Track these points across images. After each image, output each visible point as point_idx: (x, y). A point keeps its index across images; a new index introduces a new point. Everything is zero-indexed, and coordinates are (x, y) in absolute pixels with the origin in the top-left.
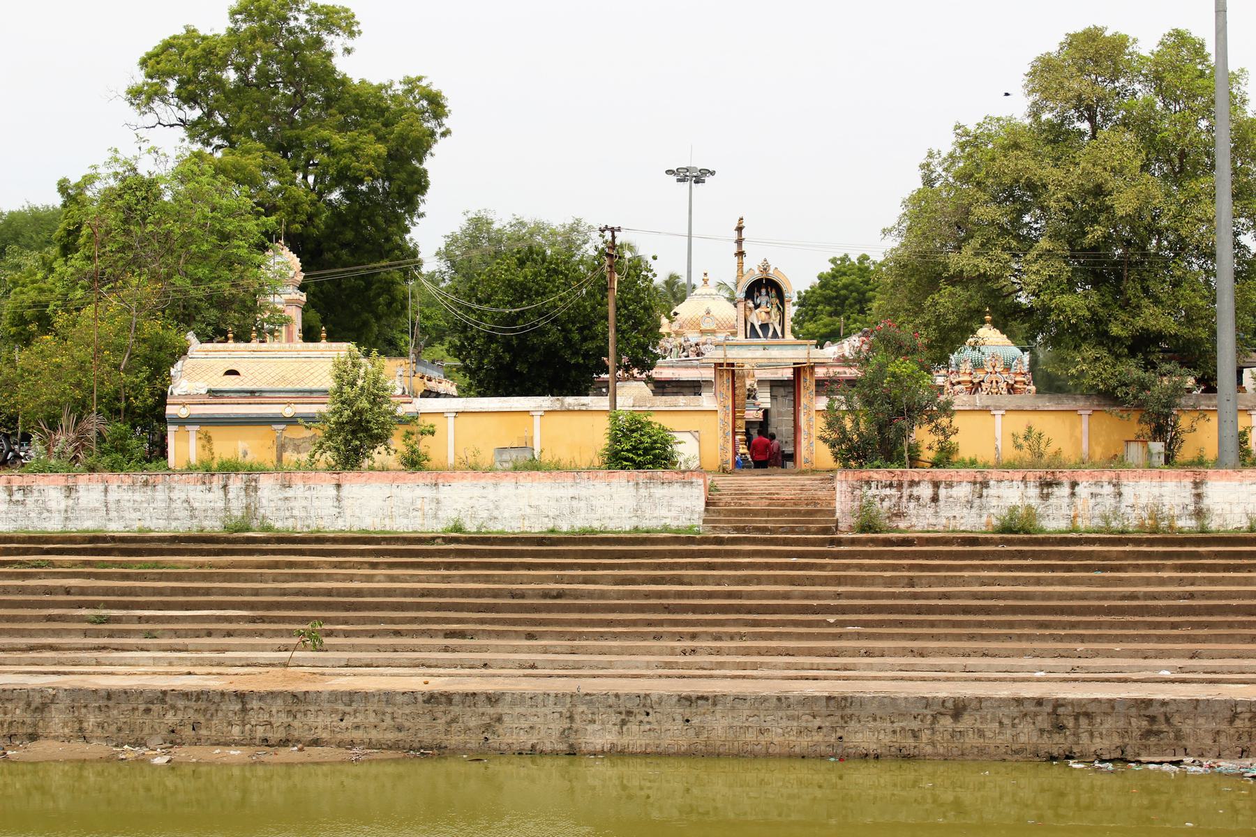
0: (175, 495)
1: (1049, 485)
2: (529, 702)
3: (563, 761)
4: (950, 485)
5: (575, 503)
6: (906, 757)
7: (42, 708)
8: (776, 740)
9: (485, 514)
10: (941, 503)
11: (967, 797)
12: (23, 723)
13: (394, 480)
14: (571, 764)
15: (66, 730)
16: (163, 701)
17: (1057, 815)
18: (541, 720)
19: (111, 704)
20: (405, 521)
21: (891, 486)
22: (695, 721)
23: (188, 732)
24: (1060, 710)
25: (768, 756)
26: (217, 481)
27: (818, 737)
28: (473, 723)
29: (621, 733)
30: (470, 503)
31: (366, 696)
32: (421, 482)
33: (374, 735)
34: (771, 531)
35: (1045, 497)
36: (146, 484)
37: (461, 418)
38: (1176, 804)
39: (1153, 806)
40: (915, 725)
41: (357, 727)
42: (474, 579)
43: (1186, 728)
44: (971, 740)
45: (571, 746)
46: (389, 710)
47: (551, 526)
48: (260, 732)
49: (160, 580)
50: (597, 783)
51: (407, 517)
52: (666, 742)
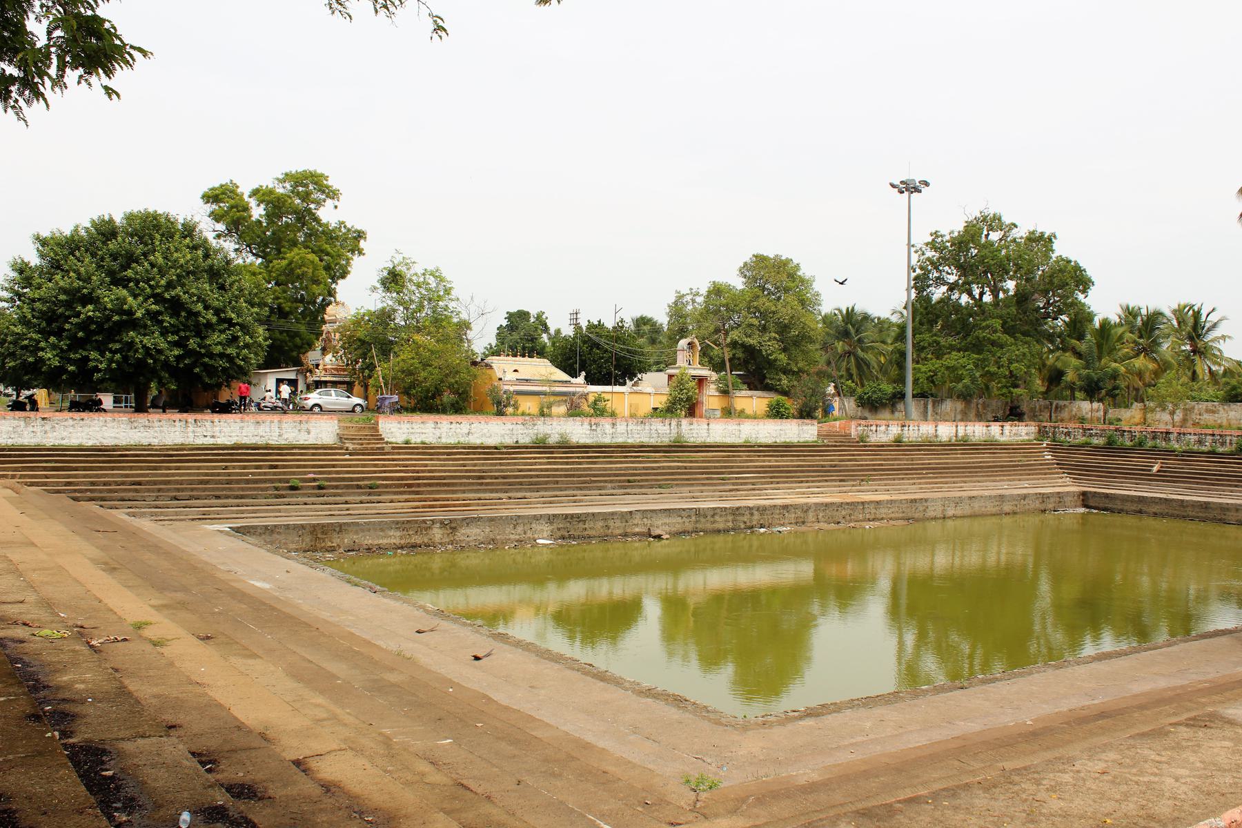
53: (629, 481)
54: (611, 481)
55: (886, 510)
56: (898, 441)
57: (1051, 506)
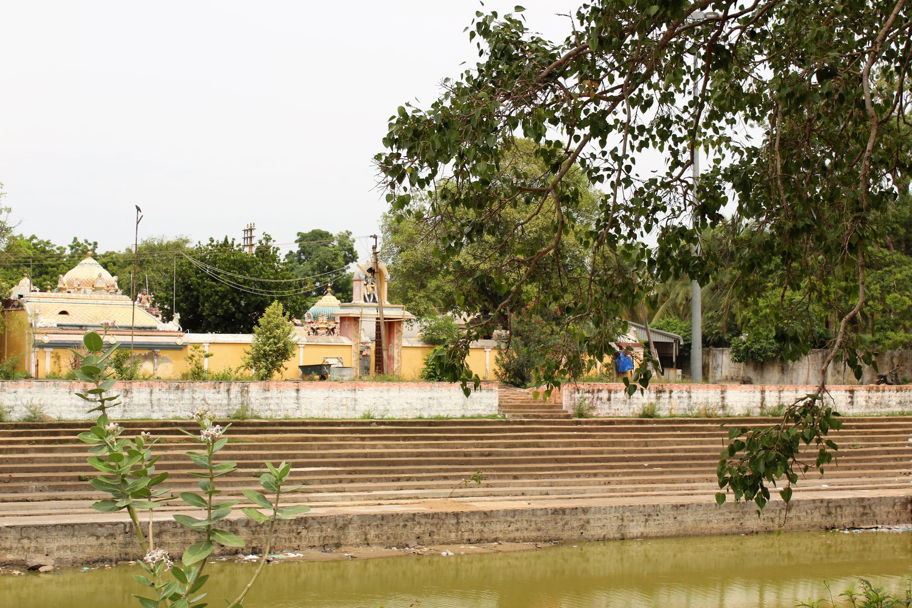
0: (195, 396)
1: (660, 392)
2: (603, 511)
3: (618, 543)
4: (616, 392)
5: (431, 401)
6: (769, 532)
7: (344, 527)
8: (715, 526)
9: (382, 408)
10: (612, 401)
11: (793, 550)
12: (333, 537)
13: (331, 387)
14: (622, 544)
15: (358, 540)
16: (413, 520)
17: (828, 557)
18: (608, 521)
19: (384, 523)
20: (337, 412)
21: (589, 392)
22: (679, 518)
23: (426, 538)
24: (830, 505)
25: (711, 535)
26: (223, 387)
27: (732, 524)
28: (575, 524)
29: (645, 526)
30: (373, 401)
31: (522, 512)
32: (346, 388)
33: (526, 534)
34: (542, 417)
35: (658, 398)
36: (178, 388)
37: (310, 349)
38: (873, 549)
39: (864, 550)
40: (772, 515)
41: (517, 530)
42: (431, 446)
43: (877, 511)
44: (795, 522)
45: (622, 535)
46: (534, 519)
47: (418, 415)
48: (466, 536)
49: (249, 450)
50: (634, 554)
51: (338, 409)
52: (666, 530)
53: (80, 479)
54: (37, 479)
55: (503, 526)
56: (648, 415)
57: (846, 521)
